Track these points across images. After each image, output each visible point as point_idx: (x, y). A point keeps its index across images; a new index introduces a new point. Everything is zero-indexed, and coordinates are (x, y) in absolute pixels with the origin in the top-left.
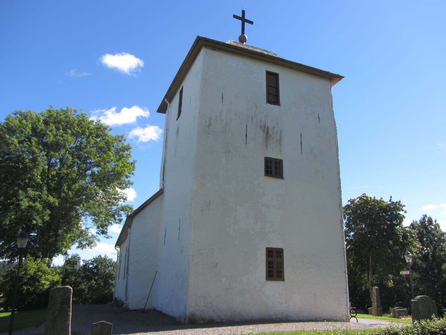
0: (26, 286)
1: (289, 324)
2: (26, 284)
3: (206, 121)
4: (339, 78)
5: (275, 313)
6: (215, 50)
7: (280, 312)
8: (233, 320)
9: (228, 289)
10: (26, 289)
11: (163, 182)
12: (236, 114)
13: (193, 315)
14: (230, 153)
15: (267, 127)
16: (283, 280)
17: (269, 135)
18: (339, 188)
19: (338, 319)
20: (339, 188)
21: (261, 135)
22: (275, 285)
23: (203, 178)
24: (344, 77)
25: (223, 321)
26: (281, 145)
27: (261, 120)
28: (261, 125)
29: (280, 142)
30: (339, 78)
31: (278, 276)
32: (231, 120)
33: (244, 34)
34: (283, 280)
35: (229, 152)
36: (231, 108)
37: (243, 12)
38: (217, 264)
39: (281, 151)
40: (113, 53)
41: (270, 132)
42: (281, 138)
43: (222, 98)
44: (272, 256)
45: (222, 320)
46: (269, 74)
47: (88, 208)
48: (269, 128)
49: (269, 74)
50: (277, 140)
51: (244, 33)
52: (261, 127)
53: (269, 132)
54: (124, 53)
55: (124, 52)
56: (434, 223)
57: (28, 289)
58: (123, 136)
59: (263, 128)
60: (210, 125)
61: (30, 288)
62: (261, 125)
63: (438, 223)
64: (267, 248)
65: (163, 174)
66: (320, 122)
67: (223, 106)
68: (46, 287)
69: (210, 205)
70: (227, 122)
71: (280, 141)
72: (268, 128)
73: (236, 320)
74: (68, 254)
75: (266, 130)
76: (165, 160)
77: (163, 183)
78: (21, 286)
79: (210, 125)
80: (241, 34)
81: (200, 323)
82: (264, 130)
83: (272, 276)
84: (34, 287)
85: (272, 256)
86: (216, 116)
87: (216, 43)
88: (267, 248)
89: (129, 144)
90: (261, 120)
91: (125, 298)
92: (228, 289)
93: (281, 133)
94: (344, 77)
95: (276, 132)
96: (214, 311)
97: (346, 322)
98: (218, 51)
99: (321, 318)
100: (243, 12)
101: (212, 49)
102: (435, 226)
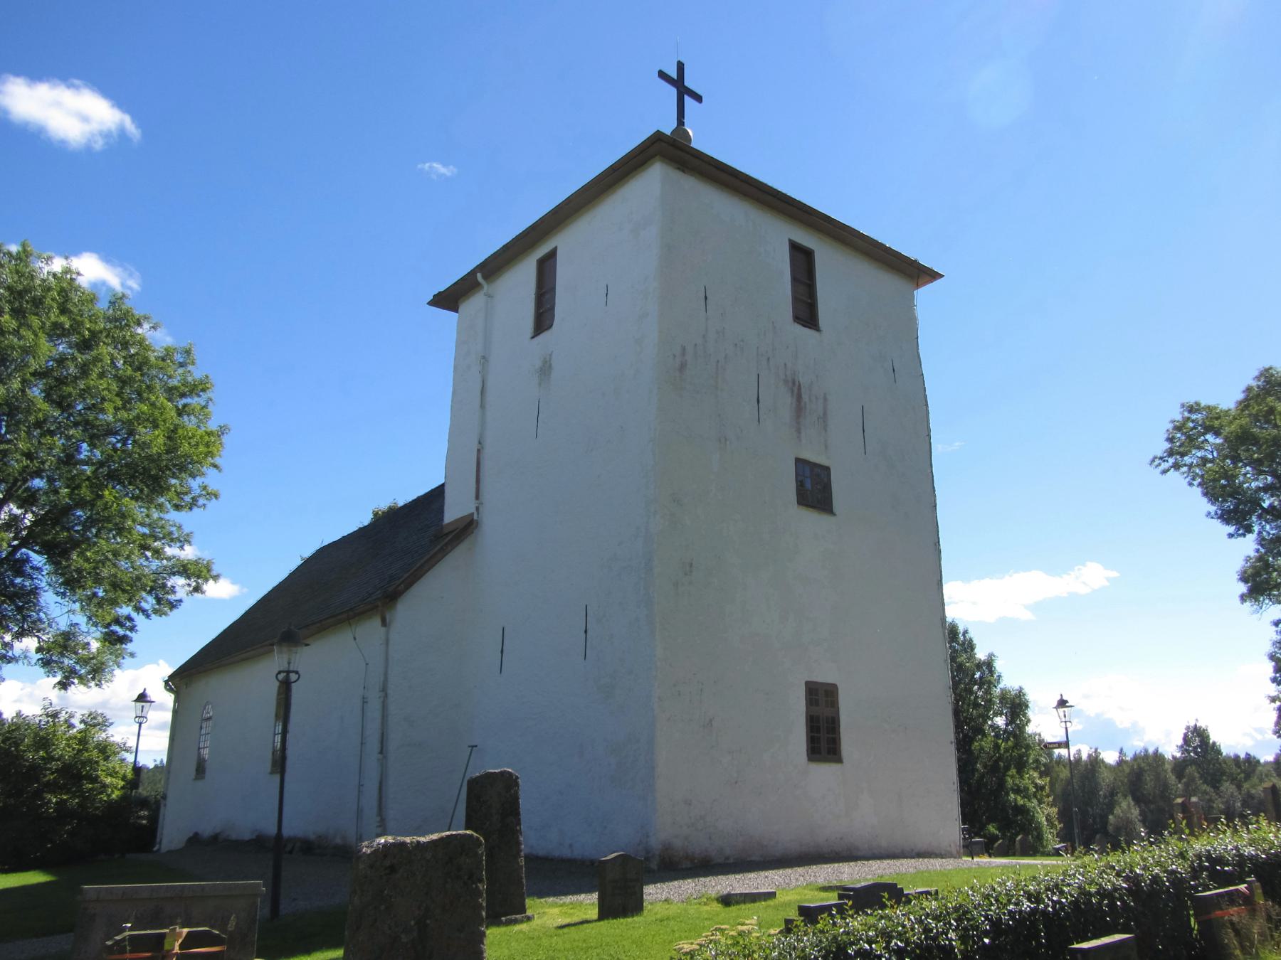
0: (53, 792)
1: (752, 875)
2: (53, 787)
3: (675, 356)
4: (933, 276)
5: (827, 840)
6: (683, 171)
7: (836, 838)
8: (748, 859)
9: (736, 782)
10: (57, 802)
11: (477, 501)
12: (736, 345)
13: (667, 847)
14: (728, 443)
15: (797, 383)
16: (839, 760)
17: (803, 404)
18: (935, 545)
19: (943, 852)
20: (935, 545)
21: (786, 402)
22: (824, 771)
23: (674, 501)
24: (942, 276)
25: (729, 862)
26: (826, 431)
27: (785, 365)
28: (786, 376)
29: (824, 421)
30: (933, 276)
31: (829, 753)
32: (726, 358)
33: (684, 125)
34: (839, 760)
35: (726, 440)
36: (724, 328)
37: (681, 67)
38: (711, 721)
39: (826, 447)
40: (35, 74)
41: (805, 397)
42: (825, 414)
43: (706, 298)
44: (817, 704)
45: (727, 858)
46: (795, 247)
47: (100, 565)
48: (802, 386)
49: (795, 247)
50: (818, 418)
51: (684, 122)
52: (786, 381)
53: (803, 396)
54: (77, 82)
55: (78, 78)
56: (962, 638)
57: (61, 803)
58: (190, 349)
59: (790, 384)
60: (683, 367)
61: (65, 801)
62: (786, 376)
63: (971, 640)
64: (807, 683)
65: (475, 480)
66: (897, 381)
67: (707, 319)
68: (116, 795)
69: (691, 572)
70: (718, 361)
71: (824, 419)
72: (800, 385)
73: (754, 858)
74: (149, 699)
75: (797, 391)
76: (480, 443)
77: (477, 505)
78: (38, 794)
79: (683, 367)
80: (675, 125)
81: (684, 867)
82: (792, 392)
83: (820, 753)
84: (78, 797)
85: (817, 704)
86: (696, 345)
87: (693, 155)
88: (807, 683)
89: (207, 377)
90: (785, 365)
91: (378, 819)
92: (736, 782)
93: (825, 400)
94: (942, 276)
95: (817, 398)
96: (710, 838)
97: (955, 858)
98: (692, 175)
99: (913, 850)
100: (681, 67)
101: (678, 169)
102: (963, 644)
